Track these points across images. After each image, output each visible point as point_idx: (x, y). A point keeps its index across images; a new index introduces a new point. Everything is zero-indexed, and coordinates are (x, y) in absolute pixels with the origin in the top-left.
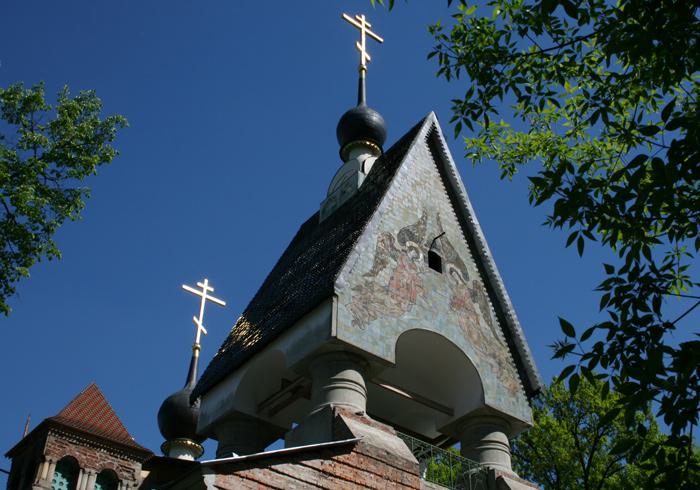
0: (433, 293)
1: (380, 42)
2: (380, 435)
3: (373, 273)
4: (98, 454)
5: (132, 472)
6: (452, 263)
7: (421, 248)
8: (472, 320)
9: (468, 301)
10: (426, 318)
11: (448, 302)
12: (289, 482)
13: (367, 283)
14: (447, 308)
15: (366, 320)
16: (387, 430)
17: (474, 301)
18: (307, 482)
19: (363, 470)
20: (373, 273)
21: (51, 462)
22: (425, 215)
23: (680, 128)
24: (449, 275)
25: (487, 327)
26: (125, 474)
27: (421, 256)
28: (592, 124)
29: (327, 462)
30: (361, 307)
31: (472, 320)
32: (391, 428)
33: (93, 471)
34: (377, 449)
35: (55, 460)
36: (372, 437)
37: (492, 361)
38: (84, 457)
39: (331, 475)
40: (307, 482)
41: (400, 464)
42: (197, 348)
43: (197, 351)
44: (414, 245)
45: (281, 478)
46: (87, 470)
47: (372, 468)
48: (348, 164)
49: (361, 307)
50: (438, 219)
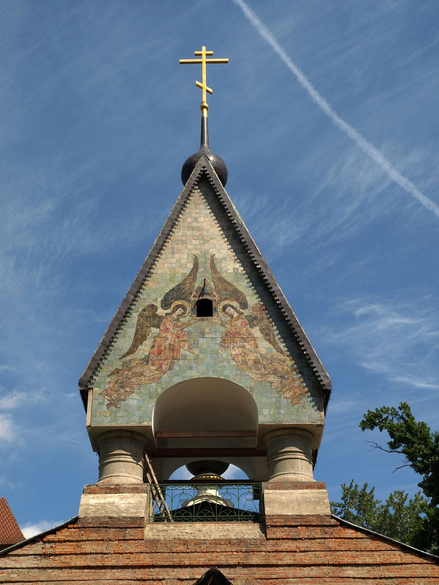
1: (226, 62)
3: (131, 351)
13: (125, 364)
19: (85, 541)
20: (131, 351)
23: (89, 392)
27: (189, 309)
37: (272, 378)
39: (51, 555)
42: (205, 107)
43: (205, 110)
47: (94, 536)
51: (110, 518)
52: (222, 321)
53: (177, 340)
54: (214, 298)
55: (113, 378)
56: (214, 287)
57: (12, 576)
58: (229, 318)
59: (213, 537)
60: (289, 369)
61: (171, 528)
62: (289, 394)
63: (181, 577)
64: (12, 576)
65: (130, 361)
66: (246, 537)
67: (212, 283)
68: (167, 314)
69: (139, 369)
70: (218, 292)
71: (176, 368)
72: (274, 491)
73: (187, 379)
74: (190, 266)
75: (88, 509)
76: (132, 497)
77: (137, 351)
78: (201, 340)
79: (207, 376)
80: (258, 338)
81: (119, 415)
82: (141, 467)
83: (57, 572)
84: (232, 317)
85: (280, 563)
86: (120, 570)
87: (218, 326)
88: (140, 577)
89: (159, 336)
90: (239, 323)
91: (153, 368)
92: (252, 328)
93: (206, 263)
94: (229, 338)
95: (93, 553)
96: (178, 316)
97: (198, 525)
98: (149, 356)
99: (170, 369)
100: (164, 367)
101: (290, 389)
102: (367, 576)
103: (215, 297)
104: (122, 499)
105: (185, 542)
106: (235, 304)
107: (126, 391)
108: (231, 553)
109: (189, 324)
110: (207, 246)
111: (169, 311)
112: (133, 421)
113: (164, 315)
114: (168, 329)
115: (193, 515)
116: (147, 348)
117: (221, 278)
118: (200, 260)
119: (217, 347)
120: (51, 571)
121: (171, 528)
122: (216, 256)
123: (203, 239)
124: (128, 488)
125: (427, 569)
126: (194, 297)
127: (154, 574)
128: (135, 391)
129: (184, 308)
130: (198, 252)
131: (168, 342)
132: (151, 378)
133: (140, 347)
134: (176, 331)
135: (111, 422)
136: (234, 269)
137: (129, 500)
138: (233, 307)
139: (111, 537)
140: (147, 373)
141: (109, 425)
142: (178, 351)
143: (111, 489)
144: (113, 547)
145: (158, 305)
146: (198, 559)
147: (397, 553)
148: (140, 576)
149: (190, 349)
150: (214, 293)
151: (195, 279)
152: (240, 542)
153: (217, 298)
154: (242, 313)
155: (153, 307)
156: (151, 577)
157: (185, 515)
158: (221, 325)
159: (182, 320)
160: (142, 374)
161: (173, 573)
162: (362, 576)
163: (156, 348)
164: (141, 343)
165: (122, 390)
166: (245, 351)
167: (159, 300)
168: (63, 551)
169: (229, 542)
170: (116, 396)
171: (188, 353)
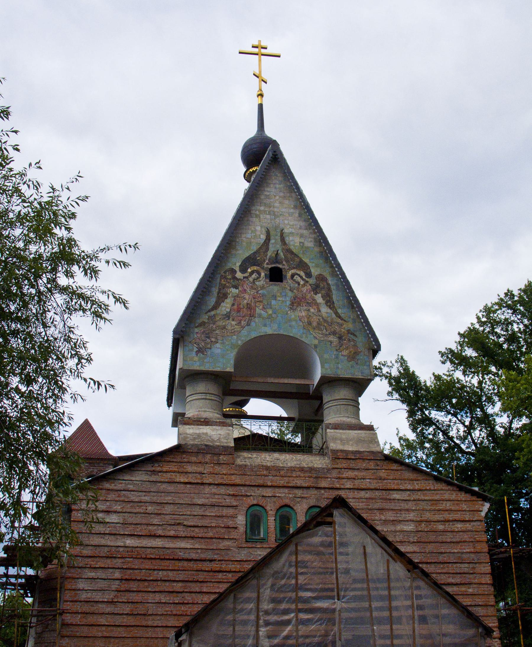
10: (265, 325)
13: (210, 318)
22: (268, 238)
25: (329, 311)
27: (263, 274)
37: (332, 338)
39: (160, 472)
45: (121, 483)
51: (206, 445)
52: (290, 287)
53: (253, 301)
54: (284, 267)
55: (200, 329)
56: (283, 257)
57: (129, 486)
58: (297, 285)
59: (289, 465)
60: (346, 332)
61: (254, 456)
62: (345, 353)
63: (264, 494)
64: (129, 486)
65: (214, 315)
66: (315, 466)
67: (282, 254)
68: (244, 277)
69: (221, 323)
70: (287, 261)
71: (253, 324)
72: (335, 431)
73: (262, 334)
74: (263, 237)
75: (187, 438)
76: (221, 430)
77: (220, 308)
78: (273, 302)
79: (279, 333)
80: (320, 303)
81: (205, 361)
83: (164, 486)
84: (299, 284)
85: (342, 487)
86: (216, 487)
87: (288, 291)
88: (232, 493)
89: (238, 296)
90: (304, 289)
91: (234, 323)
92: (316, 295)
93: (276, 235)
94: (296, 303)
95: (194, 473)
96: (254, 279)
97: (276, 455)
98: (230, 312)
99: (248, 324)
100: (243, 323)
101: (347, 349)
102: (408, 498)
103: (283, 266)
104: (213, 430)
105: (267, 468)
106: (302, 274)
107: (212, 341)
108: (304, 478)
109: (263, 288)
110: (277, 220)
111: (246, 275)
112: (218, 367)
113: (242, 278)
114: (245, 290)
115: (286, 447)
116: (228, 305)
117: (290, 249)
118: (272, 233)
119: (287, 309)
120: (160, 484)
121: (254, 456)
122: (286, 231)
123: (274, 215)
124: (216, 422)
125: (452, 494)
126: (267, 264)
128: (219, 341)
129: (259, 274)
130: (269, 226)
131: (245, 302)
132: (233, 331)
133: (222, 304)
134: (252, 293)
135: (200, 366)
136: (300, 243)
137: (219, 432)
139: (207, 460)
140: (229, 327)
141: (198, 368)
142: (255, 310)
143: (202, 422)
144: (207, 469)
145: (237, 269)
147: (431, 482)
149: (264, 308)
150: (284, 263)
151: (267, 249)
152: (311, 469)
153: (286, 267)
154: (307, 282)
155: (233, 271)
156: (240, 494)
157: (280, 447)
158: (290, 290)
159: (257, 283)
160: (224, 327)
161: (258, 492)
162: (405, 499)
163: (235, 307)
164: (223, 302)
165: (208, 340)
166: (310, 314)
167: (238, 264)
169: (302, 469)
170: (203, 344)
171: (262, 312)
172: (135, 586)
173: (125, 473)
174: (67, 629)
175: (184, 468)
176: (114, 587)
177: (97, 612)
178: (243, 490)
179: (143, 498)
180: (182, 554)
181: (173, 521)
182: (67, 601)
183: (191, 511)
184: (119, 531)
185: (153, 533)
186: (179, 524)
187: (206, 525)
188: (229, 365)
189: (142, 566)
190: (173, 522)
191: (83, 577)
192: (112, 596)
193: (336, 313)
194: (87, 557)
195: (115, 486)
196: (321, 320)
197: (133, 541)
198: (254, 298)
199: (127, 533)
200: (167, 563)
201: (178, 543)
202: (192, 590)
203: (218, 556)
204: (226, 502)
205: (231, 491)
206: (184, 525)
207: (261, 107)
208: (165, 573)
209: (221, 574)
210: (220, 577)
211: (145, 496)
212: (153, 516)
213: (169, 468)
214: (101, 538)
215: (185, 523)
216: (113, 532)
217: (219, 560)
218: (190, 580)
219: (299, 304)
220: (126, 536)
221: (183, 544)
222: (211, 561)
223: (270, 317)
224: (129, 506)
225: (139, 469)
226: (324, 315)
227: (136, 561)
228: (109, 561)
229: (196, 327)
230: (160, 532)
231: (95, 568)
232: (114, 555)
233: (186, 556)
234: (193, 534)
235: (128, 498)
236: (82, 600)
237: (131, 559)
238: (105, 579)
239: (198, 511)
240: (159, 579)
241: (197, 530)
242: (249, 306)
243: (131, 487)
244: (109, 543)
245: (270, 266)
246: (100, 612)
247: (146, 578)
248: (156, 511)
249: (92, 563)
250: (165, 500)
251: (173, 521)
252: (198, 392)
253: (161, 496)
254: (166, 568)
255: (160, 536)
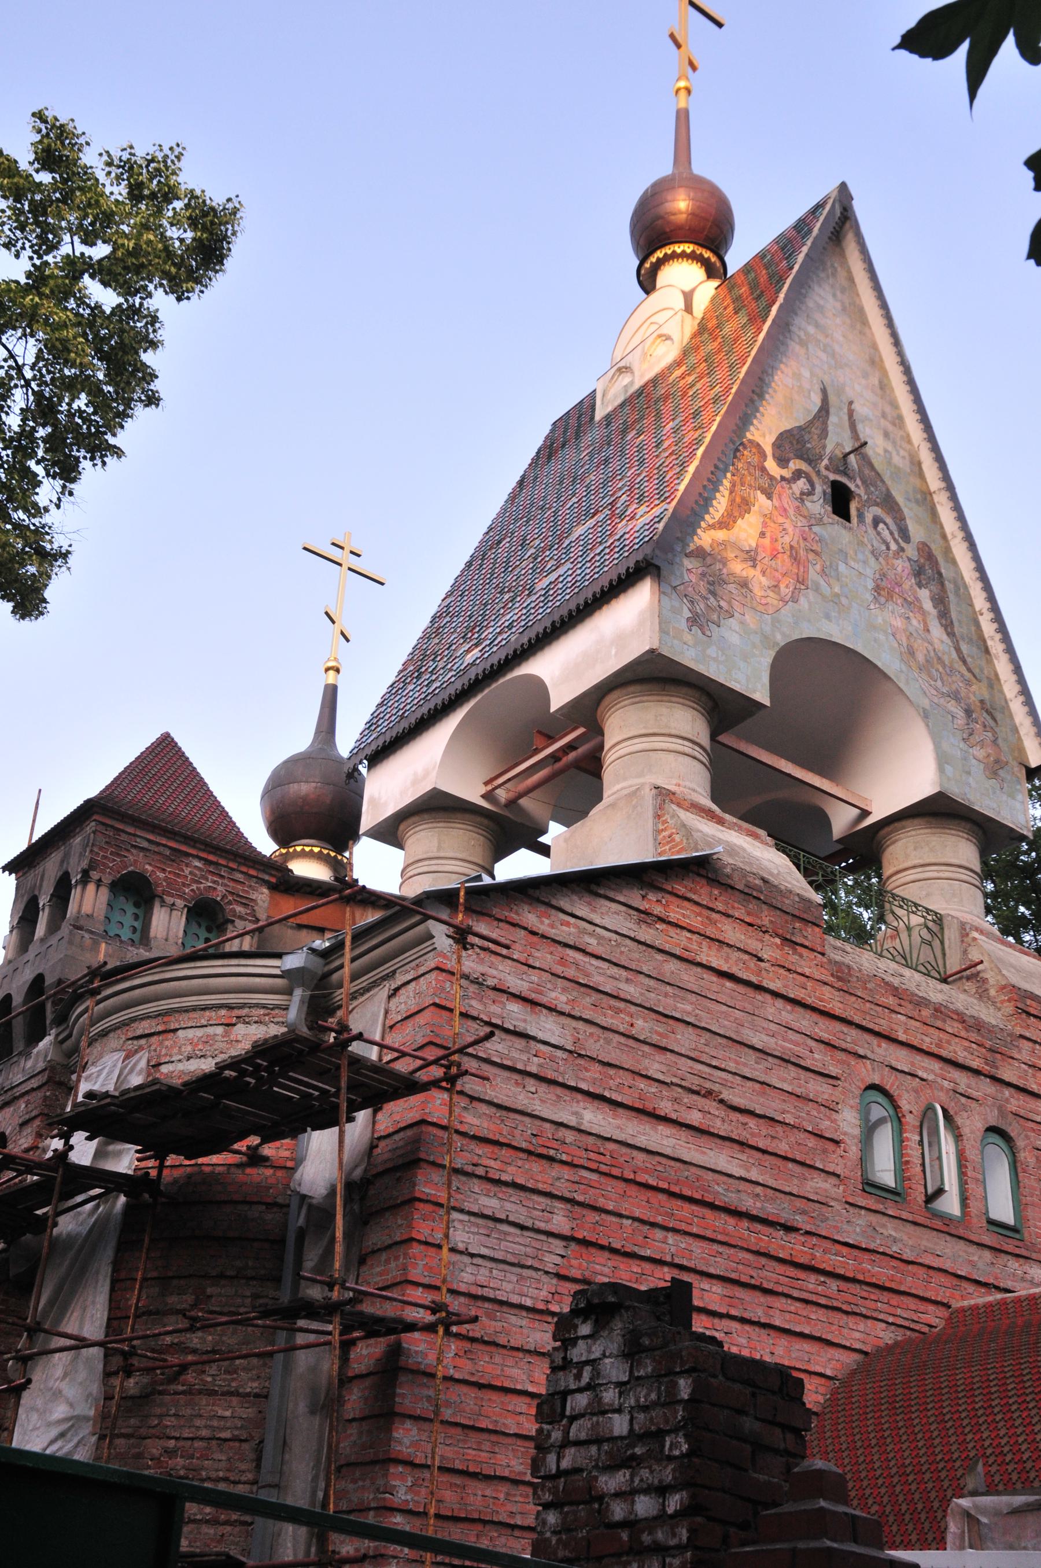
0: (842, 567)
2: (745, 845)
4: (187, 871)
5: (247, 903)
6: (877, 504)
7: (818, 473)
8: (914, 622)
9: (910, 583)
10: (828, 617)
11: (870, 584)
12: (584, 932)
14: (869, 597)
15: (715, 617)
16: (756, 836)
17: (920, 585)
18: (616, 933)
21: (99, 883)
22: (824, 410)
24: (871, 531)
25: (945, 637)
26: (239, 909)
27: (818, 489)
28: (678, 112)
29: (652, 897)
30: (704, 592)
31: (914, 622)
32: (762, 833)
33: (180, 903)
34: (744, 873)
35: (107, 880)
36: (732, 850)
37: (952, 706)
38: (161, 875)
39: (661, 920)
40: (616, 933)
41: (787, 904)
44: (803, 466)
45: (568, 924)
46: (169, 900)
48: (654, 296)
49: (704, 592)
50: (851, 413)
56: (856, 466)
58: (884, 548)
63: (894, 1064)
74: (816, 400)
82: (702, 762)
84: (888, 548)
88: (825, 1036)
107: (721, 607)
127: (849, 1039)
138: (886, 524)
146: (919, 1036)
148: (826, 1036)
158: (872, 552)
168: (685, 922)
172: (606, 1270)
173: (573, 892)
174: (416, 1391)
175: (718, 928)
176: (551, 1261)
177: (502, 1340)
178: (851, 1037)
179: (623, 986)
180: (722, 1192)
181: (697, 1081)
182: (417, 1284)
183: (737, 1063)
184: (562, 1074)
185: (649, 1107)
186: (709, 1094)
187: (770, 1113)
188: (759, 686)
189: (625, 1208)
190: (693, 1082)
191: (467, 1206)
192: (544, 1294)
193: (958, 650)
194: (474, 1137)
195: (552, 926)
196: (932, 654)
197: (600, 1117)
198: (805, 539)
199: (584, 1086)
200: (686, 1211)
201: (711, 1153)
202: (747, 1315)
203: (806, 1218)
204: (813, 1059)
205: (824, 1029)
206: (722, 1101)
207: (683, 118)
208: (684, 1242)
209: (813, 1278)
210: (811, 1286)
211: (627, 980)
212: (646, 1049)
213: (684, 915)
214: (517, 1084)
215: (725, 1095)
216: (550, 1075)
217: (808, 1233)
218: (744, 1279)
219: (890, 597)
220: (579, 1096)
221: (721, 1159)
222: (789, 1229)
223: (835, 599)
224: (588, 1000)
225: (611, 894)
226: (937, 644)
227: (611, 1186)
228: (536, 1166)
229: (687, 555)
230: (665, 1107)
231: (498, 1182)
232: (552, 1153)
233: (731, 1199)
234: (744, 1135)
235: (587, 975)
236: (463, 1288)
237: (594, 1177)
238: (523, 1228)
239: (751, 1065)
240: (668, 1259)
241: (752, 1123)
242: (794, 552)
243: (591, 943)
244: (539, 1109)
245: (832, 477)
246: (513, 1344)
247: (636, 1249)
248: (655, 1039)
249: (492, 1163)
250: (676, 1009)
251: (697, 1081)
252: (673, 732)
253: (666, 995)
254: (683, 1226)
255: (665, 1120)
